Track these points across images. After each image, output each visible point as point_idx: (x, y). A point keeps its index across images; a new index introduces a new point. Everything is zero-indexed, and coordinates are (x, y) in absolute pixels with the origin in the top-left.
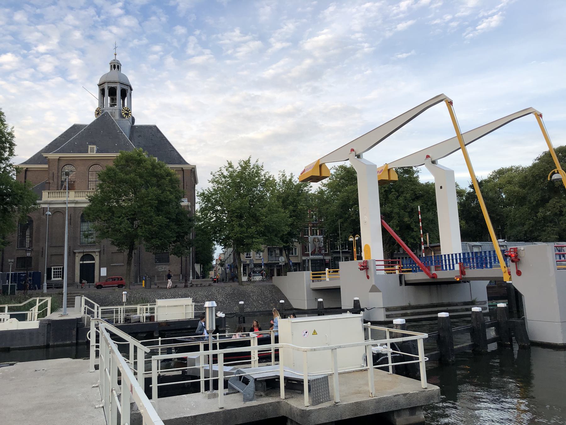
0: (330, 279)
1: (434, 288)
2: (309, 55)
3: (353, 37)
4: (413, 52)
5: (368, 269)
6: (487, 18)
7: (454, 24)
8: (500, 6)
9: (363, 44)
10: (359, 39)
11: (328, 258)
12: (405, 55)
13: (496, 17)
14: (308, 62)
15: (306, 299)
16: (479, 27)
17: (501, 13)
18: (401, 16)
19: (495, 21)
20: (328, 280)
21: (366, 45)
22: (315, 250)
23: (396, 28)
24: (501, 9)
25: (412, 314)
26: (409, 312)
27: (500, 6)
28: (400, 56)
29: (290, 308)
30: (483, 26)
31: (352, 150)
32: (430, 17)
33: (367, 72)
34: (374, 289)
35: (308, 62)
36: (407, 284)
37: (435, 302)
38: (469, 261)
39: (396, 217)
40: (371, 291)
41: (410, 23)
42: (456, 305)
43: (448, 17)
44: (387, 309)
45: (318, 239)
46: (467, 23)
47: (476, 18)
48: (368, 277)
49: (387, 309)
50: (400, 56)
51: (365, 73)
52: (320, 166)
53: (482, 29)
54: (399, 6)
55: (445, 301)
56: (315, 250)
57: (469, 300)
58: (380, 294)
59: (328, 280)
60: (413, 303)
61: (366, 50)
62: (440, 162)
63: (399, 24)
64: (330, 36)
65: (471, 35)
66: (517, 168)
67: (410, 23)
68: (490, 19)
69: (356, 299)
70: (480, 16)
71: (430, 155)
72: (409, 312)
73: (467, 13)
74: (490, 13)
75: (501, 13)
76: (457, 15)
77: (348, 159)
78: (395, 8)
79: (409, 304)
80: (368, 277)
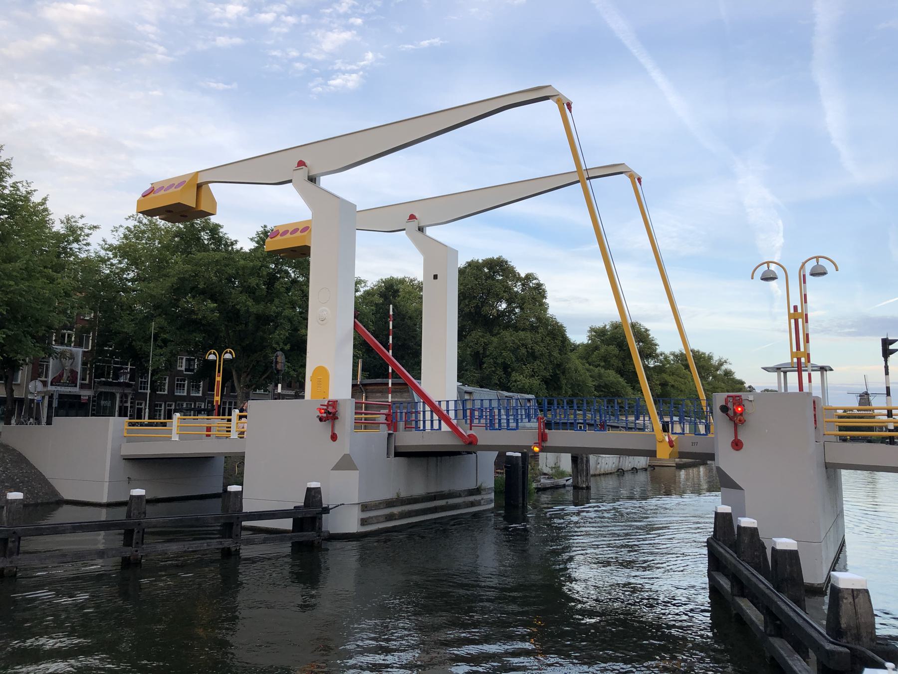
0: (181, 437)
1: (433, 460)
2: (48, 28)
3: (140, 28)
4: (235, 85)
5: (742, 422)
6: (344, 73)
7: (300, 66)
8: (362, 63)
9: (156, 46)
10: (152, 36)
11: (86, 394)
12: (221, 86)
13: (354, 76)
14: (46, 40)
15: (107, 479)
16: (331, 82)
17: (361, 73)
18: (226, 25)
19: (352, 81)
20: (175, 437)
21: (161, 49)
22: (61, 376)
23: (214, 40)
24: (363, 68)
25: (403, 515)
26: (396, 510)
27: (362, 63)
28: (213, 85)
29: (53, 500)
30: (337, 82)
31: (301, 164)
32: (268, 43)
33: (155, 93)
34: (345, 464)
35: (46, 40)
36: (398, 454)
37: (433, 489)
38: (472, 411)
39: (288, 326)
40: (337, 467)
41: (237, 41)
42: (457, 495)
43: (294, 53)
44: (365, 507)
45: (71, 354)
46: (317, 71)
47: (330, 68)
48: (334, 437)
49: (365, 507)
50: (213, 85)
51: (150, 93)
52: (199, 186)
53: (335, 86)
54: (224, 10)
55: (445, 488)
56: (61, 376)
57: (472, 486)
58: (354, 475)
59: (175, 437)
60: (403, 494)
61: (159, 57)
62: (430, 231)
63: (220, 36)
64: (98, 12)
65: (320, 89)
66: (411, 281)
67: (237, 41)
68: (347, 76)
69: (314, 485)
70: (336, 67)
71: (417, 215)
72: (396, 510)
73: (320, 57)
74: (349, 68)
75: (361, 73)
76: (307, 55)
77: (290, 181)
78: (217, 9)
79: (398, 494)
80: (334, 437)
